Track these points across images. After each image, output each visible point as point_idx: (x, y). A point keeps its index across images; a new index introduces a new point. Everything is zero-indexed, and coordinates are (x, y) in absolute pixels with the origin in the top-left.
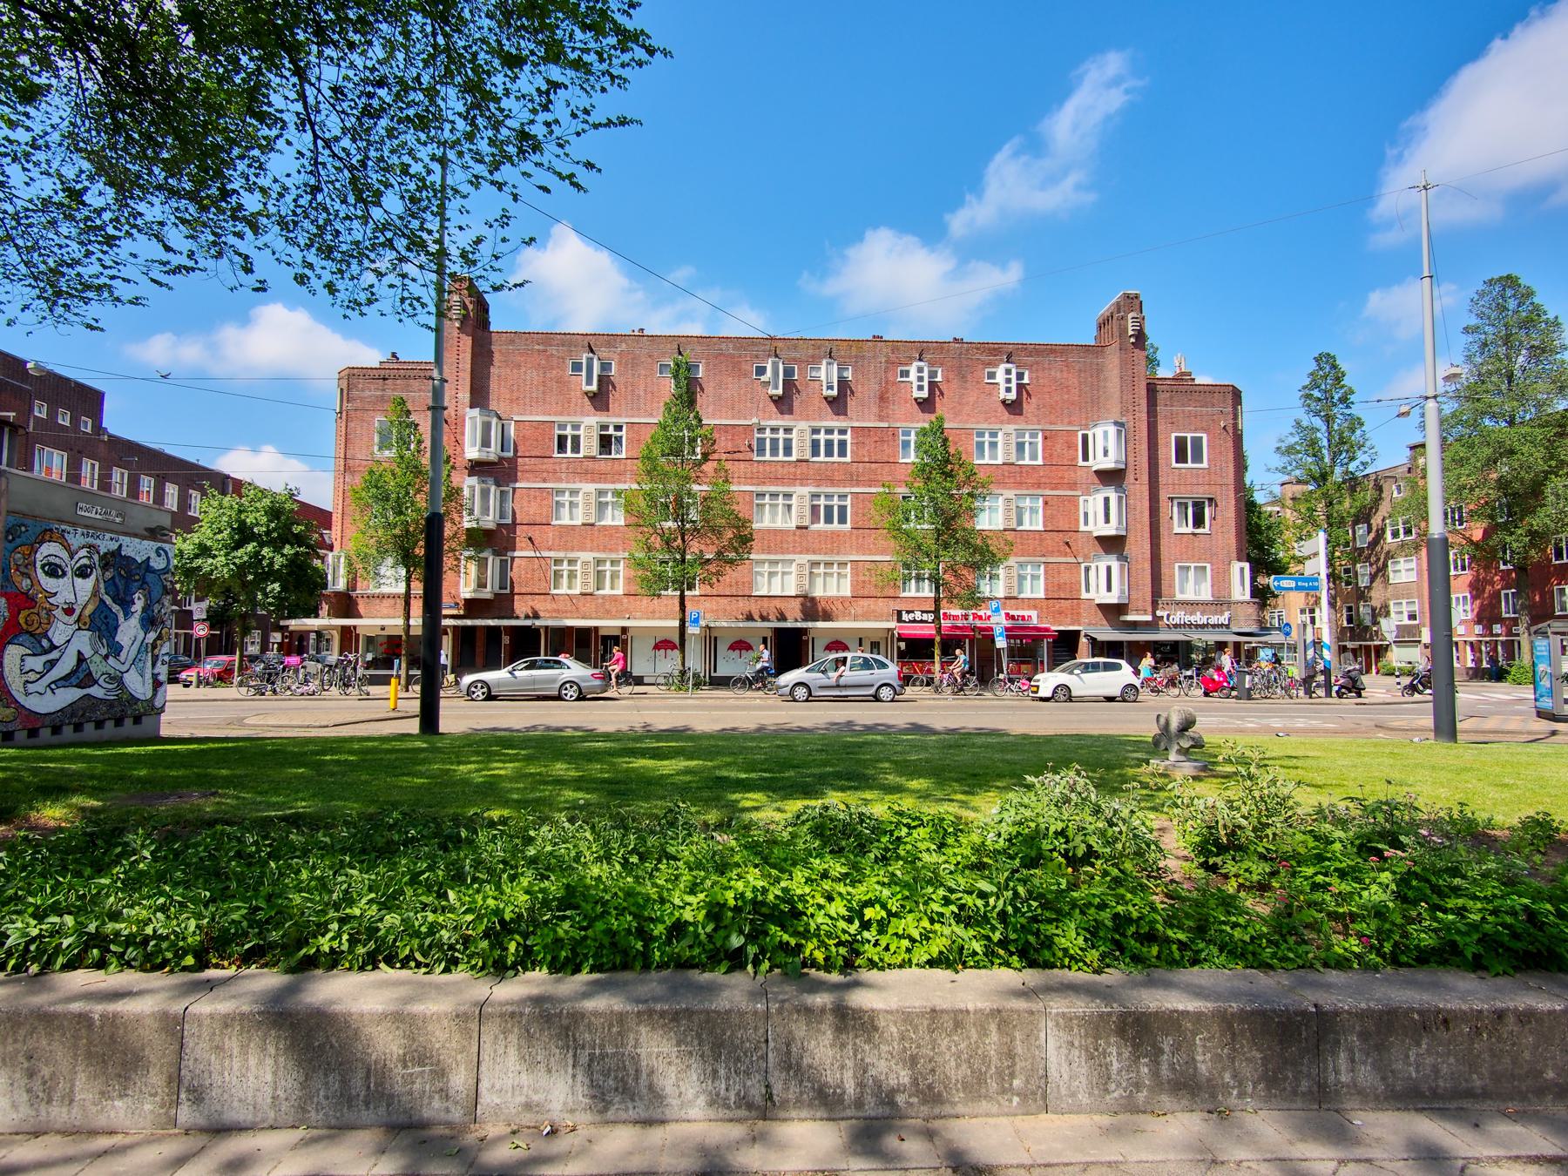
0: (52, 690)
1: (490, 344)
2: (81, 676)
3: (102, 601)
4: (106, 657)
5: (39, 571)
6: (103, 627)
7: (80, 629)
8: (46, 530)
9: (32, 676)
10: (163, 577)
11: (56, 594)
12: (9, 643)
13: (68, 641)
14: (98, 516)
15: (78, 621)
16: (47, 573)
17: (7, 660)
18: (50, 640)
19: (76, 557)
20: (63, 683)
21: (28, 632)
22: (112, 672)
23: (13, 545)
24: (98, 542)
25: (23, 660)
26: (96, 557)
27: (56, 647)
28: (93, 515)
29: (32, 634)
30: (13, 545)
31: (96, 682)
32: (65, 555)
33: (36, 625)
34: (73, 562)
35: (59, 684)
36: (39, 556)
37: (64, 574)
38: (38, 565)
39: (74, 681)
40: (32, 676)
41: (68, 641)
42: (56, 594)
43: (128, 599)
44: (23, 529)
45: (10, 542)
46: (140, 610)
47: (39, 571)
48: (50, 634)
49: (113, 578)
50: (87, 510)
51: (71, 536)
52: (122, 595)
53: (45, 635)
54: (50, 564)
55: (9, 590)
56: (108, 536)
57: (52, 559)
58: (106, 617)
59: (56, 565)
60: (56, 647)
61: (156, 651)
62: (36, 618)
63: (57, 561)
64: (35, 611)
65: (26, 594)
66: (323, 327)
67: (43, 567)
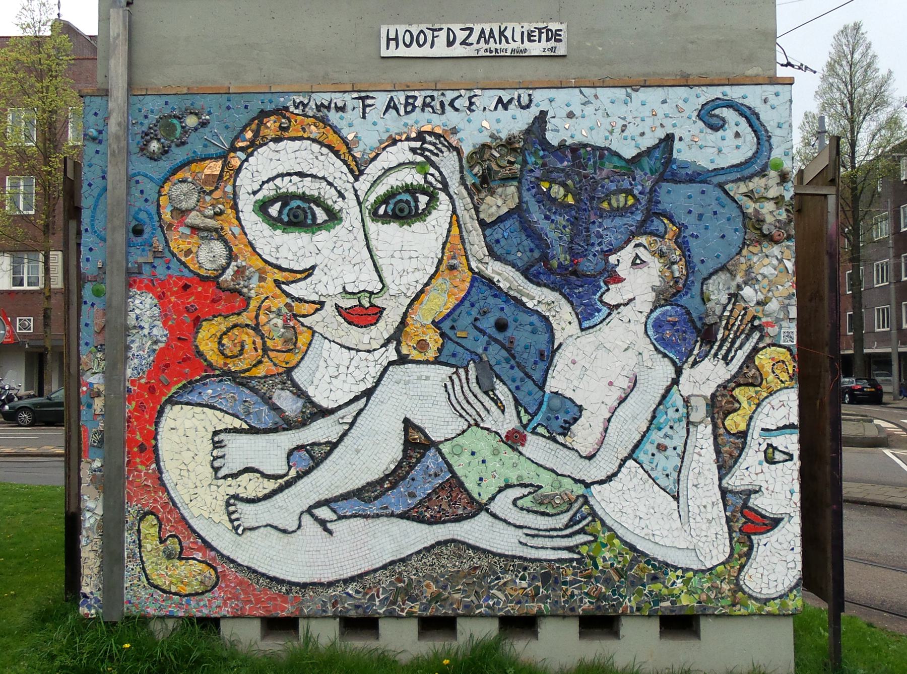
0: (323, 523)
1: (66, 569)
2: (424, 489)
3: (480, 279)
4: (514, 440)
5: (249, 217)
6: (495, 354)
7: (403, 360)
8: (263, 114)
9: (251, 486)
10: (738, 190)
11: (309, 272)
12: (172, 401)
13: (368, 393)
14: (458, 50)
15: (397, 336)
16: (275, 222)
17: (167, 443)
18: (300, 393)
19: (373, 170)
20: (355, 505)
21: (228, 373)
22: (545, 480)
23: (165, 165)
24: (452, 118)
25: (217, 445)
26: (449, 164)
27: (325, 413)
28: (441, 49)
29: (240, 380)
30: (165, 165)
31: (477, 508)
32: (334, 168)
33: (250, 356)
34: (363, 185)
35: (345, 508)
36: (246, 182)
37: (334, 217)
38: (246, 204)
39: (396, 500)
40: (251, 486)
41: (368, 393)
42: (309, 272)
43: (588, 265)
44: (191, 121)
45: (153, 158)
46: (645, 300)
47: (249, 217)
48: (297, 375)
49: (518, 212)
50: (415, 40)
51: (353, 115)
52: (560, 256)
53: (287, 377)
54: (285, 198)
55: (161, 272)
56: (487, 99)
57: (268, 191)
58: (501, 326)
59: (303, 197)
60: (325, 413)
61: (736, 422)
62: (248, 337)
63: (309, 187)
64: (245, 318)
65: (213, 280)
66: (671, 642)
67: (262, 208)
